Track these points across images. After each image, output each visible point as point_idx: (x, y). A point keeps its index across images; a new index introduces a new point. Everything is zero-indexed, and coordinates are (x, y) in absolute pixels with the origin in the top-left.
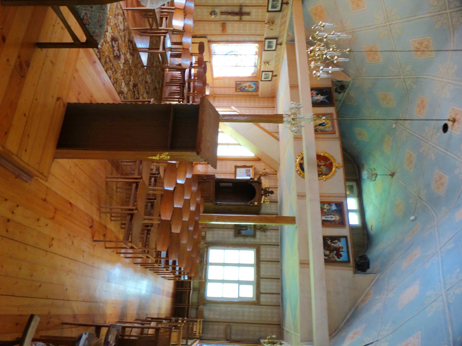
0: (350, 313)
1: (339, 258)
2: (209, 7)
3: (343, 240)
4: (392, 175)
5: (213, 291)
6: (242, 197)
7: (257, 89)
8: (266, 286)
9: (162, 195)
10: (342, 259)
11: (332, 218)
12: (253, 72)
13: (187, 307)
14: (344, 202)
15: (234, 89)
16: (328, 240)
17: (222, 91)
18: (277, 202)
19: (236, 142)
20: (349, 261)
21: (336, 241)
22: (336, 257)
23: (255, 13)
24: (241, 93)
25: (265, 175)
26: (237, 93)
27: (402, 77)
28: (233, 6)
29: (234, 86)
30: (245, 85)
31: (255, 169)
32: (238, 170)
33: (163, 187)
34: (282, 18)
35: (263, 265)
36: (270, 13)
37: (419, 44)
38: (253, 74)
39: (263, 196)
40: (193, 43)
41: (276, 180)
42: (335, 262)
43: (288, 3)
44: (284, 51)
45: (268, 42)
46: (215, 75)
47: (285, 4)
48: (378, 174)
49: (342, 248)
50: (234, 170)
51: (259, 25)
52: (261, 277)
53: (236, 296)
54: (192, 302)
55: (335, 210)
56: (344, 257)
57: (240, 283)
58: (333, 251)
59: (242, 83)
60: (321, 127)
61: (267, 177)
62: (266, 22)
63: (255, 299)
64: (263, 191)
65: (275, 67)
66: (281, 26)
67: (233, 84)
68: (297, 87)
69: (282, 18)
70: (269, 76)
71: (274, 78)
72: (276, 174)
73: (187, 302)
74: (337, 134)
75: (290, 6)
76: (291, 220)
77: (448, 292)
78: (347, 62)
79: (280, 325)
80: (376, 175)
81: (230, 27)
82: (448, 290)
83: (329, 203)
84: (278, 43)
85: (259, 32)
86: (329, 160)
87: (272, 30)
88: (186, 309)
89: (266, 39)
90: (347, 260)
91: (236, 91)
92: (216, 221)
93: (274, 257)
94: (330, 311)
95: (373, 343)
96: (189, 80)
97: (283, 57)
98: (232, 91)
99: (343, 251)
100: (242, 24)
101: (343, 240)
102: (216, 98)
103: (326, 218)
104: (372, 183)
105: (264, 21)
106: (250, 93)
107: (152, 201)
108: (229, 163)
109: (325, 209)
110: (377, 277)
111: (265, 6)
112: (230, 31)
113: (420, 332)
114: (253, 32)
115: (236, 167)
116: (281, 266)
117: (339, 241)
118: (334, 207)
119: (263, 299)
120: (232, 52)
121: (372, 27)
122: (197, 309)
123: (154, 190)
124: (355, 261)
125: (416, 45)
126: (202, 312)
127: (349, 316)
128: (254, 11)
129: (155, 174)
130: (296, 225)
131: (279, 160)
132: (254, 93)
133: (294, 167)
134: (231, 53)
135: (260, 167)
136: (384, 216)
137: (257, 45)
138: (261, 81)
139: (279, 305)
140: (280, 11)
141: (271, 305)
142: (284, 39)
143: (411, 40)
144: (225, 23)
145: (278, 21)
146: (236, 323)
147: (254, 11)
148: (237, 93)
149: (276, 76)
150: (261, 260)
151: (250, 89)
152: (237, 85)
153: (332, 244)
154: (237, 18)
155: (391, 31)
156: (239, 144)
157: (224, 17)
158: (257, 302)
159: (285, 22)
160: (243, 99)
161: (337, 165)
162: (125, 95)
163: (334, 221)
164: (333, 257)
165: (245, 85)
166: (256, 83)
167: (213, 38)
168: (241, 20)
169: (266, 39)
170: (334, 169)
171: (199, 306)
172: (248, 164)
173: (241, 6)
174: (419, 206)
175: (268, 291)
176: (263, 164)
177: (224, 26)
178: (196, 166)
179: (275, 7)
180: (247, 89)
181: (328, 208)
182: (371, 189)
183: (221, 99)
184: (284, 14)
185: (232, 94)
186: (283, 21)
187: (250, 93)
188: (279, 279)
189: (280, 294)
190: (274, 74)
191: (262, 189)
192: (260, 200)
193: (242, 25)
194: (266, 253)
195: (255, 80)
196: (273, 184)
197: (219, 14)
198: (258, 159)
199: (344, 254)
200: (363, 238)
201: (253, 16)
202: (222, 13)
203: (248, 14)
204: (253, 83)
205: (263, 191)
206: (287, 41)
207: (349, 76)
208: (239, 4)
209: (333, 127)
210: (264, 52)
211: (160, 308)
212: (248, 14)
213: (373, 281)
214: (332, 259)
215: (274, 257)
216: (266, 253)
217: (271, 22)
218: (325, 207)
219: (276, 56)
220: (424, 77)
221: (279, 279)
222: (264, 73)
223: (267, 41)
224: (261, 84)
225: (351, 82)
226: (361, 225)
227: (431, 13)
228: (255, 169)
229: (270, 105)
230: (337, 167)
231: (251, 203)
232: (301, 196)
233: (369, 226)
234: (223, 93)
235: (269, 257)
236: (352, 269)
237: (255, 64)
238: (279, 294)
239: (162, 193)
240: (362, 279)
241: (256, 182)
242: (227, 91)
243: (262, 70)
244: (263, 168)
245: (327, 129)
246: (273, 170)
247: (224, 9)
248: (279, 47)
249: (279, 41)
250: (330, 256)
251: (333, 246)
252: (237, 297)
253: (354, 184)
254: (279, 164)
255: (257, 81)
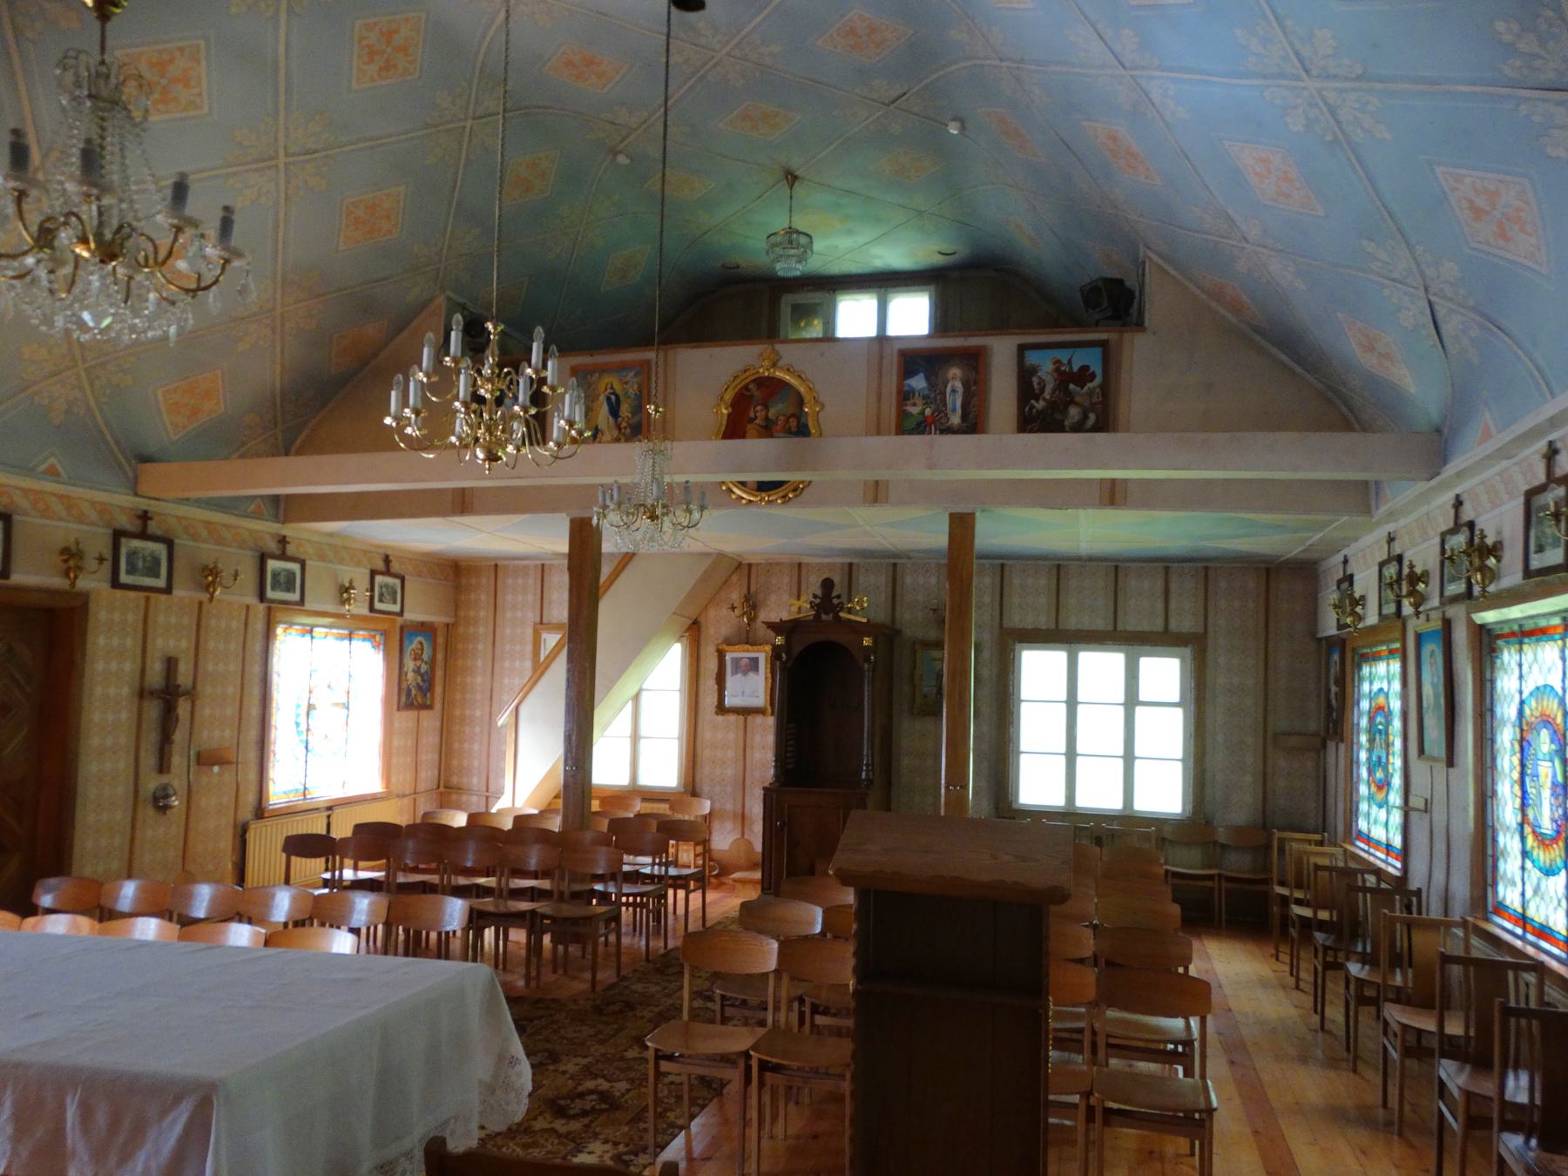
0: (1274, 351)
1: (1093, 376)
2: (140, 816)
3: (1032, 358)
4: (791, 178)
5: (1163, 793)
6: (856, 694)
7: (425, 628)
8: (1141, 611)
9: (792, 978)
10: (1097, 368)
11: (954, 391)
12: (368, 645)
13: (1224, 884)
14: (898, 346)
15: (424, 713)
16: (1033, 407)
17: (429, 757)
18: (851, 565)
19: (629, 705)
20: (1103, 344)
21: (1035, 380)
22: (1090, 385)
23: (170, 639)
24: (438, 689)
25: (751, 605)
26: (438, 706)
27: (469, 124)
28: (139, 726)
29: (412, 714)
30: (410, 675)
31: (729, 642)
32: (729, 701)
33: (766, 975)
34: (195, 537)
35: (1072, 622)
36: (307, 598)
37: (371, 61)
38: (376, 647)
39: (842, 614)
40: (287, 882)
41: (771, 566)
42: (1105, 388)
43: (146, 512)
44: (308, 532)
45: (273, 589)
46: (375, 785)
47: (145, 526)
48: (786, 225)
49: (1058, 362)
50: (732, 718)
51: (213, 622)
52: (1110, 628)
53: (1178, 714)
54: (1203, 868)
55: (928, 379)
56: (1090, 359)
57: (1132, 700)
58: (1068, 393)
59: (404, 686)
60: (625, 410)
61: (761, 597)
62: (205, 597)
63: (1187, 651)
64: (824, 617)
65: (358, 564)
66: (220, 541)
67: (406, 718)
68: (463, 492)
69: (195, 537)
70: (387, 586)
71: (396, 567)
72: (750, 565)
73: (1209, 884)
74: (650, 355)
75: (151, 506)
76: (962, 526)
77: (1314, 72)
78: (546, 332)
79: (1268, 570)
80: (791, 231)
81: (214, 735)
82: (1307, 72)
83: (905, 396)
84: (278, 552)
85: (234, 624)
86: (746, 387)
87: (236, 575)
88: (1230, 885)
89: (262, 597)
90: (1098, 351)
91: (430, 707)
92: (965, 787)
93: (1043, 582)
94: (1271, 421)
95: (1430, 303)
96: (388, 891)
97: (331, 535)
98: (430, 720)
99: (1070, 361)
100: (206, 689)
101: (1032, 358)
102: (455, 780)
103: (954, 410)
104: (818, 246)
105: (201, 603)
106: (440, 656)
107: (807, 1010)
108: (706, 734)
109: (923, 413)
110: (1155, 258)
111: (148, 599)
112: (227, 733)
113: (1439, 170)
114: (234, 647)
115: (721, 709)
116: (1079, 558)
117: (1034, 370)
118: (918, 383)
119: (1184, 623)
120: (297, 724)
121: (282, 215)
122: (1223, 846)
123: (777, 1009)
124: (1097, 324)
125: (373, 69)
126: (1238, 830)
127: (1283, 357)
128: (162, 644)
129: (802, 1015)
130: (978, 514)
131: (707, 555)
132: (440, 640)
133: (774, 511)
134: (303, 727)
135: (721, 622)
136: (920, 213)
137: (280, 630)
138: (401, 613)
139: (1205, 570)
140: (170, 544)
141: (1206, 600)
142: (266, 529)
143: (354, 86)
144: (199, 755)
145: (207, 552)
146: (1265, 717)
147: (162, 644)
148: (438, 706)
149: (387, 560)
150: (1053, 626)
151: (425, 657)
152: (410, 706)
153: (1047, 395)
154: (183, 708)
155: (308, 153)
156: (636, 698)
157: (177, 760)
158: (1192, 644)
159: (207, 523)
160: (459, 680)
161: (766, 363)
162: (621, 1148)
163: (966, 384)
164: (1091, 393)
165: (410, 675)
166: (408, 631)
167: (250, 798)
168: (192, 694)
169: (262, 597)
170: (779, 374)
171: (1215, 843)
172: (710, 664)
173: (142, 693)
174: (920, 107)
175: (1160, 606)
176: (712, 613)
177: (206, 759)
178: (716, 856)
179: (157, 562)
180: (424, 668)
181: (920, 402)
182: (836, 248)
183: (455, 763)
184: (25, 504)
185: (438, 724)
186: (204, 533)
187: (440, 656)
188: (1116, 569)
189: (1166, 566)
190: (380, 565)
191: (817, 617)
192: (858, 629)
193: (209, 689)
194: (1029, 608)
195: (397, 637)
196: (786, 580)
197: (164, 779)
198: (694, 633)
199: (1080, 359)
200: (976, 286)
201: (181, 645)
202: (163, 766)
203: (171, 663)
204: (406, 643)
205: (824, 617)
206: (276, 519)
207: (424, 305)
208: (136, 700)
209: (622, 368)
210: (308, 606)
211: (1263, 983)
212: (171, 663)
213: (1167, 273)
214: (1095, 400)
215: (1044, 581)
216: (1029, 608)
217: (208, 577)
218: (915, 410)
219: (322, 558)
220: (483, 51)
221: (1116, 568)
222: (378, 605)
223: (270, 594)
224: (412, 615)
225: (449, 293)
226: (932, 288)
227: (277, 11)
228: (729, 642)
229: (486, 580)
230: (774, 365)
231: (867, 660)
232: (876, 493)
233: (938, 260)
234: (436, 757)
235: (1042, 600)
236: (1127, 336)
237: (341, 638)
238: (1167, 570)
239: (785, 977)
240: (1158, 303)
241: (788, 640)
242: (430, 739)
243: (365, 611)
244: (725, 611)
245: (632, 390)
246: (734, 578)
247: (149, 759)
248: (291, 549)
249: (272, 546)
250: (1087, 404)
251: (1053, 392)
252: (1179, 712)
253: (787, 301)
254: (721, 556)
255: (402, 628)
